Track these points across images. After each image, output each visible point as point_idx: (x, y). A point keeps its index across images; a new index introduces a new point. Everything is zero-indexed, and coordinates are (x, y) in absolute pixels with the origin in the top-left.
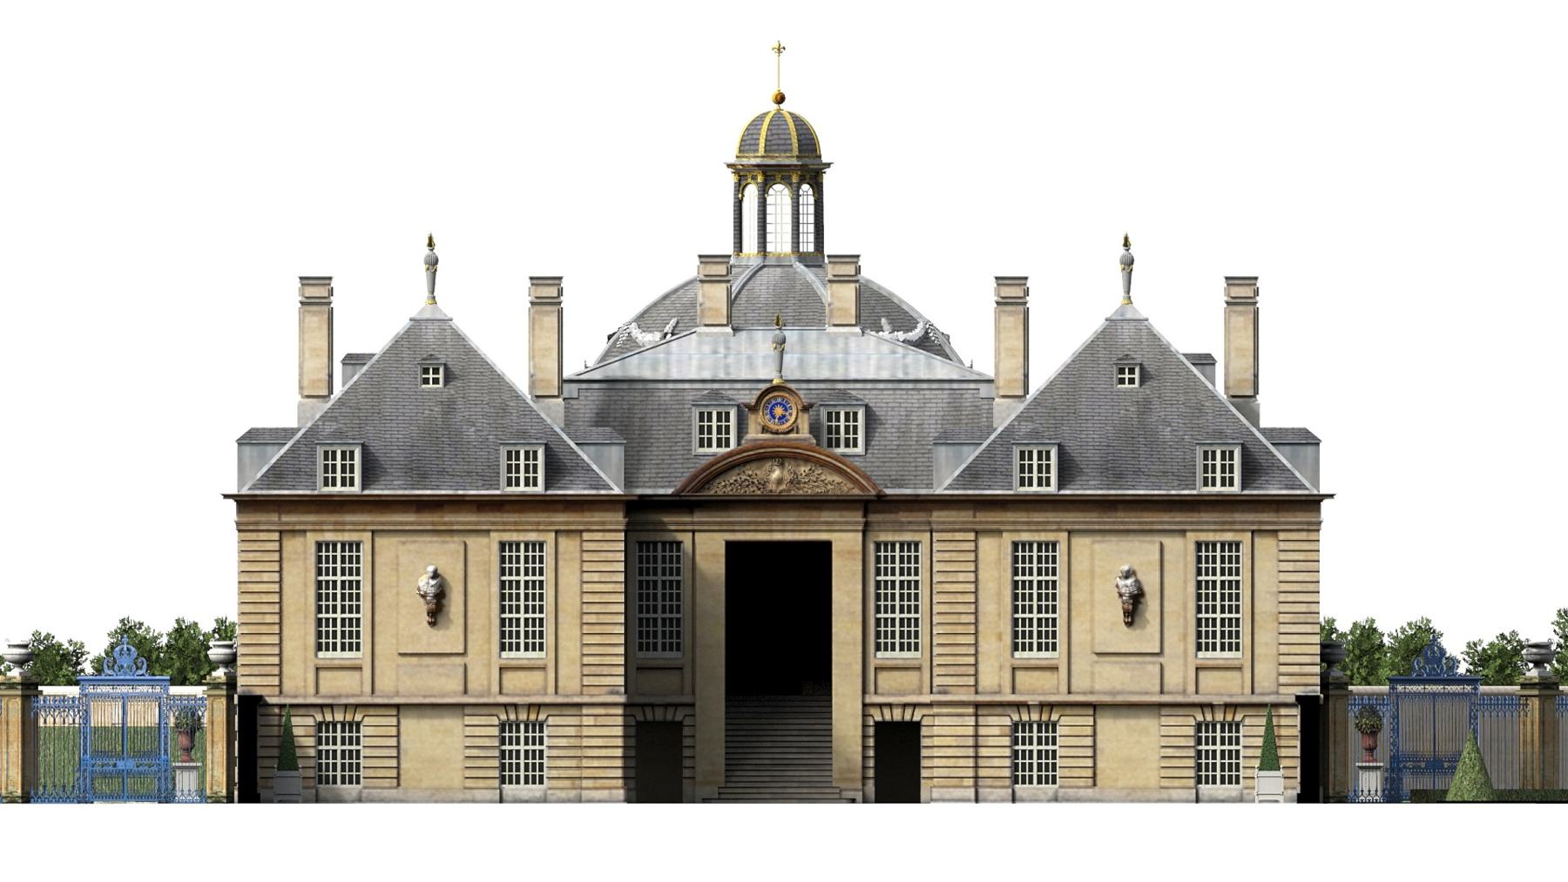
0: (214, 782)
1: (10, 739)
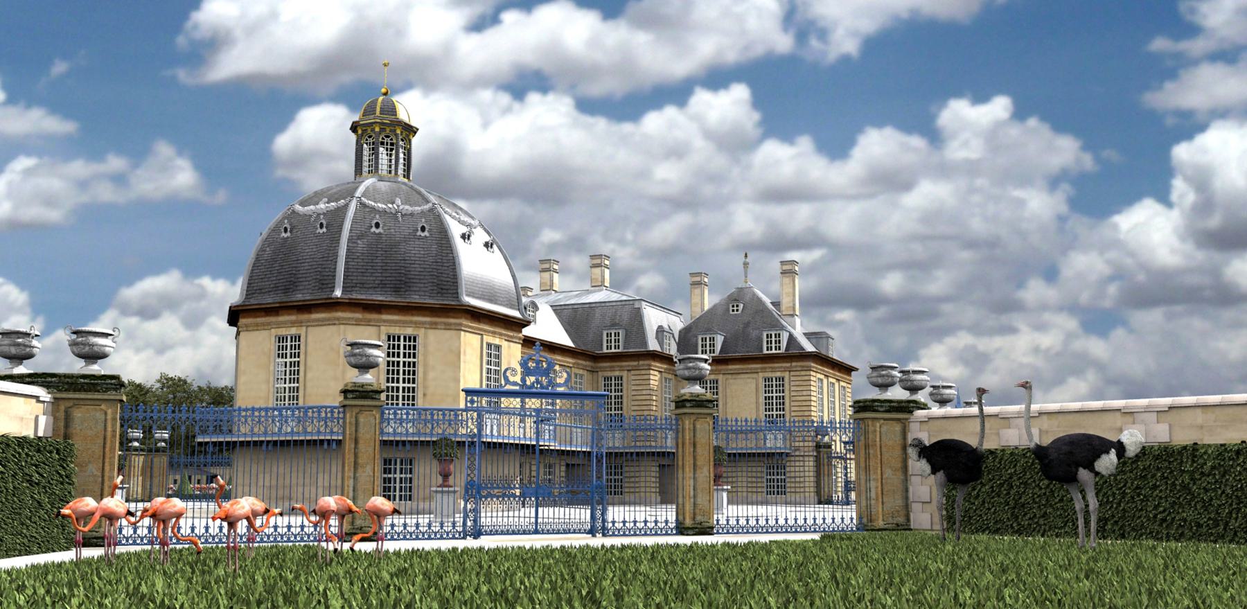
0: (697, 511)
1: (699, 463)
